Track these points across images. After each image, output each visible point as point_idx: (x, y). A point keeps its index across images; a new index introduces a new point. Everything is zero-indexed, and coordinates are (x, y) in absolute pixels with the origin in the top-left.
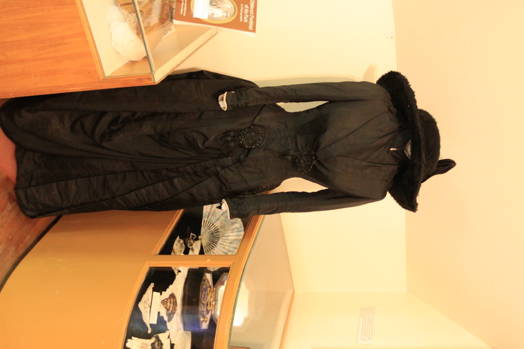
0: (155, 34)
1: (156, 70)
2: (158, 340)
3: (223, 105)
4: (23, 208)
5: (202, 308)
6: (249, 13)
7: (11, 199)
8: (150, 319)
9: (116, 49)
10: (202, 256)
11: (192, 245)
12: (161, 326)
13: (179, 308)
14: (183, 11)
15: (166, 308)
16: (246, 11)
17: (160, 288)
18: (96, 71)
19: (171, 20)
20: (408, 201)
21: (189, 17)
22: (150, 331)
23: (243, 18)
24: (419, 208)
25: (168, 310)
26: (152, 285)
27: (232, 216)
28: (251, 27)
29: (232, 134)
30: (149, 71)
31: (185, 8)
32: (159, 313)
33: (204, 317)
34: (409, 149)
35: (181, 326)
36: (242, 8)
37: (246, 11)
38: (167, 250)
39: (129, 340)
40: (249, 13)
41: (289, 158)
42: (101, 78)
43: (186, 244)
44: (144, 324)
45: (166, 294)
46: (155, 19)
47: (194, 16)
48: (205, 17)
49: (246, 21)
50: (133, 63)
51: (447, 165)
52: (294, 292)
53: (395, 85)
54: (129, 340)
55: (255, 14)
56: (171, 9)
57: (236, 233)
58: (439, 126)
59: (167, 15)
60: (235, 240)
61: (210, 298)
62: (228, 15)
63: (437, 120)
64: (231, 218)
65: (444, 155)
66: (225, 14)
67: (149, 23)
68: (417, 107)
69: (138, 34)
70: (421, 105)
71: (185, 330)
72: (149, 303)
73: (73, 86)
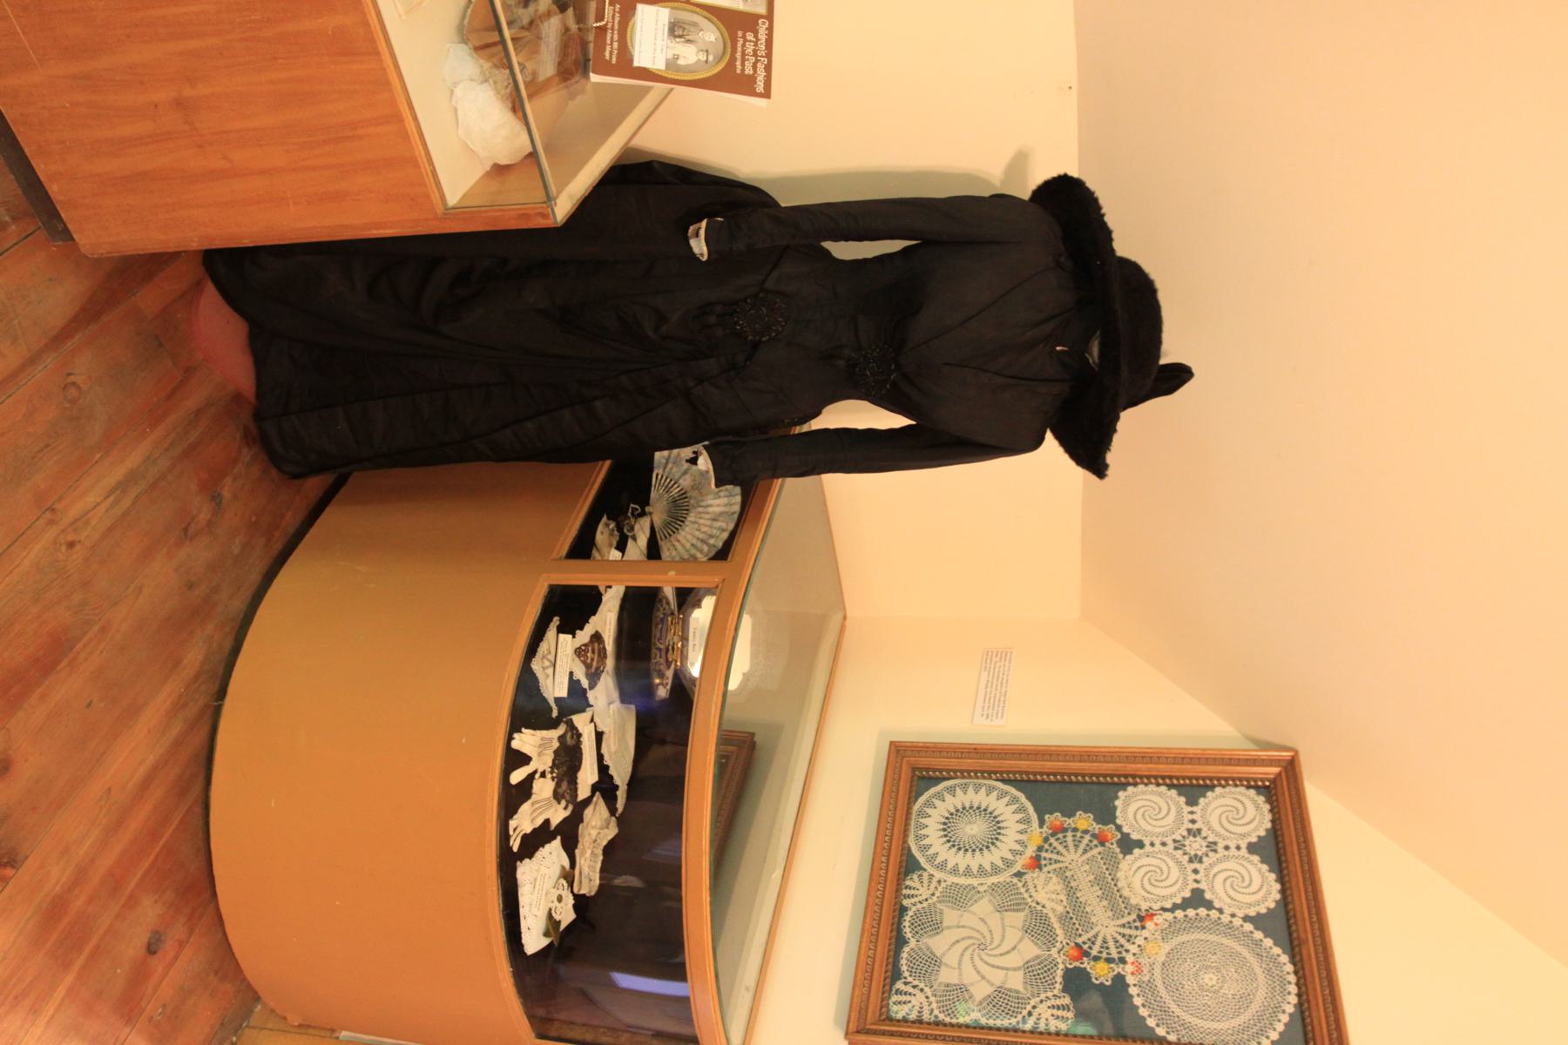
0: (550, 99)
1: (559, 192)
2: (572, 727)
3: (699, 247)
4: (274, 458)
5: (657, 659)
6: (755, 54)
7: (248, 438)
8: (555, 688)
9: (466, 137)
10: (654, 563)
11: (632, 529)
12: (577, 698)
13: (610, 662)
14: (611, 53)
15: (584, 662)
16: (750, 48)
17: (570, 627)
18: (428, 196)
19: (586, 75)
20: (1090, 452)
21: (625, 66)
22: (555, 714)
23: (743, 65)
24: (1109, 472)
25: (588, 666)
26: (556, 621)
27: (720, 482)
28: (760, 87)
29: (718, 309)
30: (541, 195)
31: (616, 45)
32: (571, 674)
33: (662, 676)
34: (1095, 350)
35: (615, 695)
36: (741, 42)
37: (750, 48)
38: (582, 548)
39: (516, 735)
40: (755, 54)
41: (841, 363)
42: (440, 210)
43: (620, 528)
44: (545, 700)
45: (584, 636)
46: (547, 66)
47: (636, 64)
48: (658, 65)
49: (749, 71)
50: (499, 170)
51: (1178, 376)
52: (845, 618)
53: (1068, 202)
54: (516, 735)
55: (769, 55)
56: (584, 45)
57: (725, 500)
58: (1163, 297)
59: (576, 63)
60: (722, 513)
61: (672, 638)
62: (711, 58)
63: (1159, 285)
64: (717, 486)
65: (1171, 352)
66: (703, 57)
67: (534, 74)
68: (1113, 250)
69: (514, 110)
70: (1123, 247)
71: (623, 701)
72: (551, 658)
73: (378, 226)
